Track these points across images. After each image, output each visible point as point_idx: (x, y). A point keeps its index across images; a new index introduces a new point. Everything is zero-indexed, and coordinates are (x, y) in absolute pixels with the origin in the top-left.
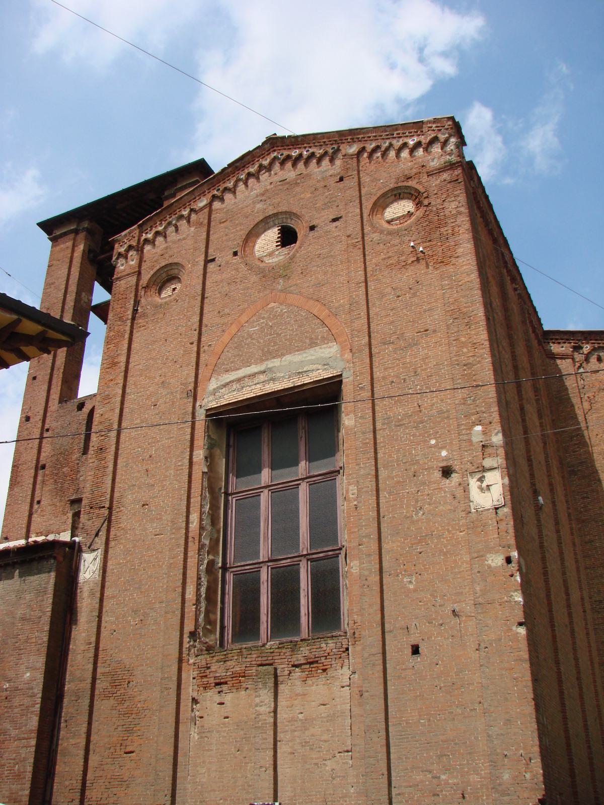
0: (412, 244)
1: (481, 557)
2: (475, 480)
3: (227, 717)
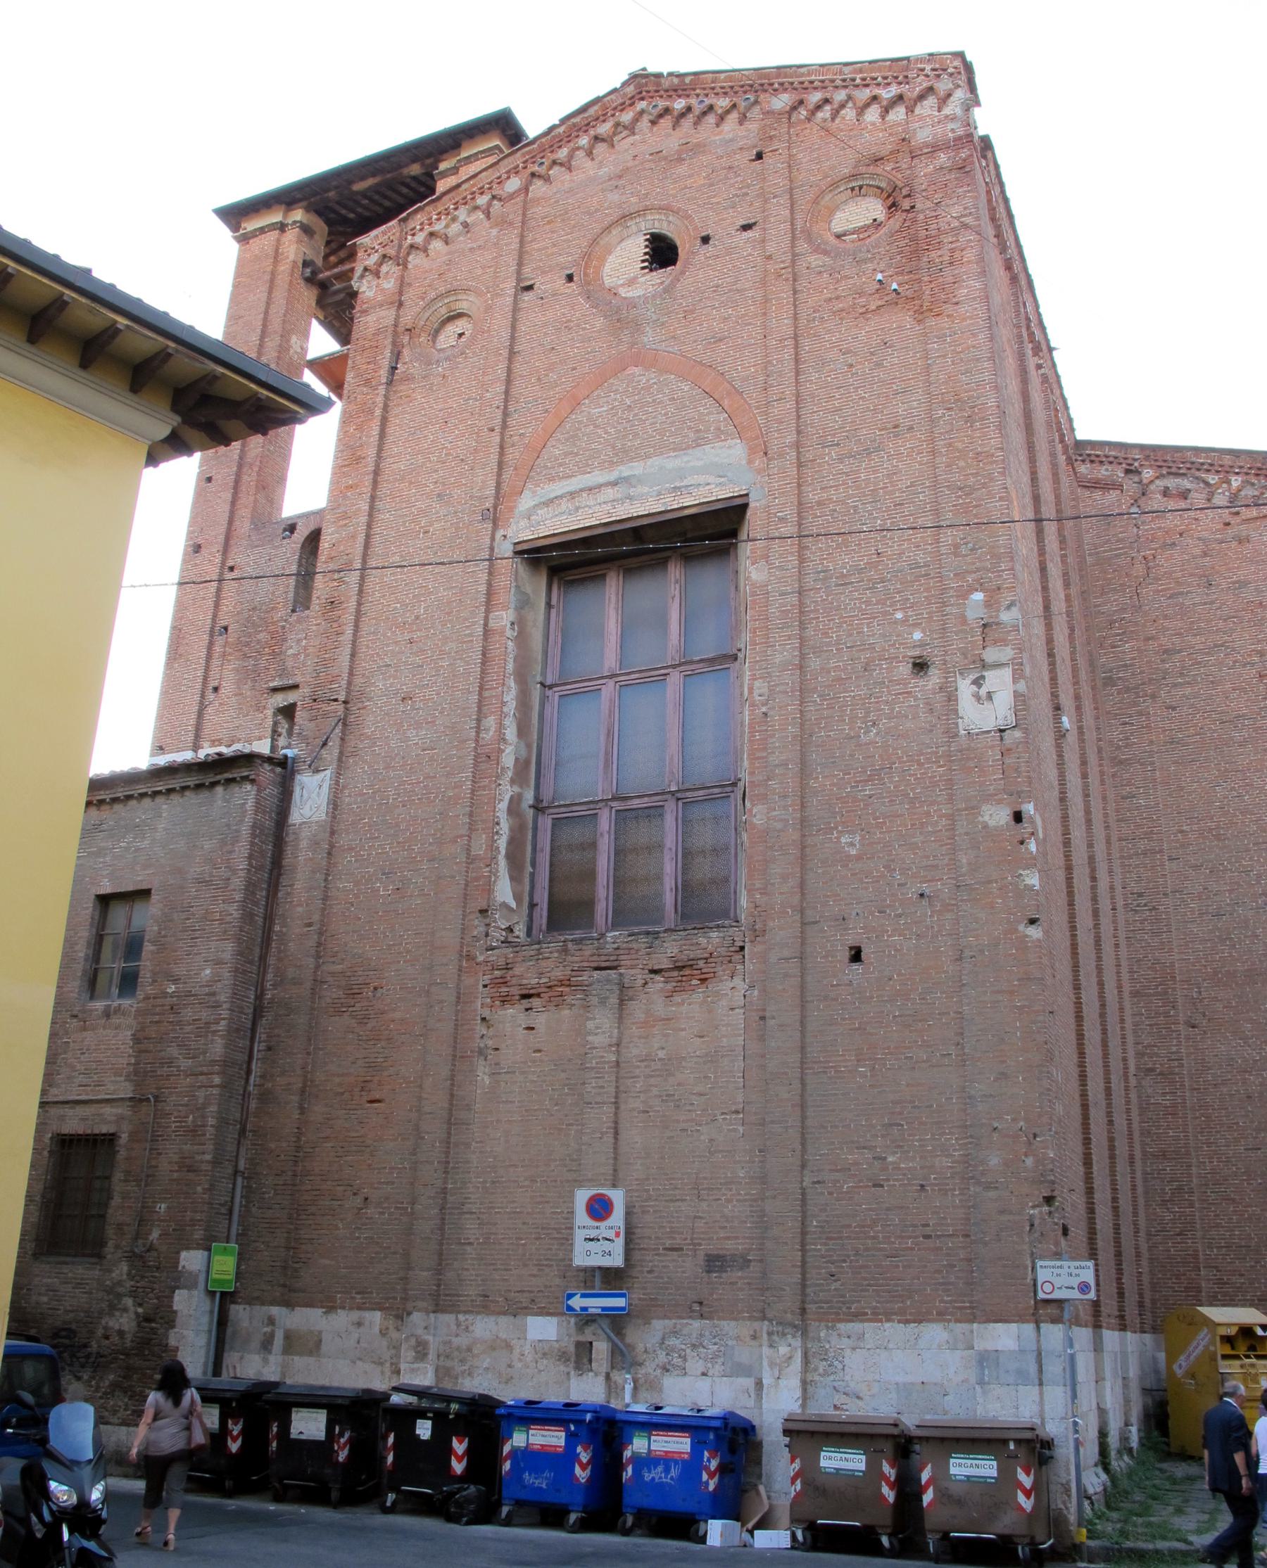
0: (879, 277)
1: (974, 810)
2: (968, 681)
3: (539, 1051)
